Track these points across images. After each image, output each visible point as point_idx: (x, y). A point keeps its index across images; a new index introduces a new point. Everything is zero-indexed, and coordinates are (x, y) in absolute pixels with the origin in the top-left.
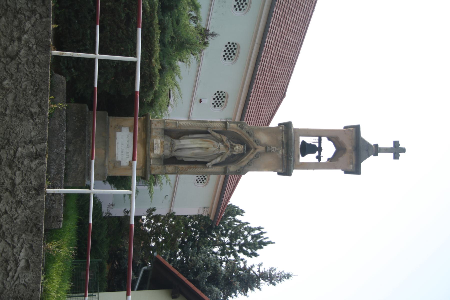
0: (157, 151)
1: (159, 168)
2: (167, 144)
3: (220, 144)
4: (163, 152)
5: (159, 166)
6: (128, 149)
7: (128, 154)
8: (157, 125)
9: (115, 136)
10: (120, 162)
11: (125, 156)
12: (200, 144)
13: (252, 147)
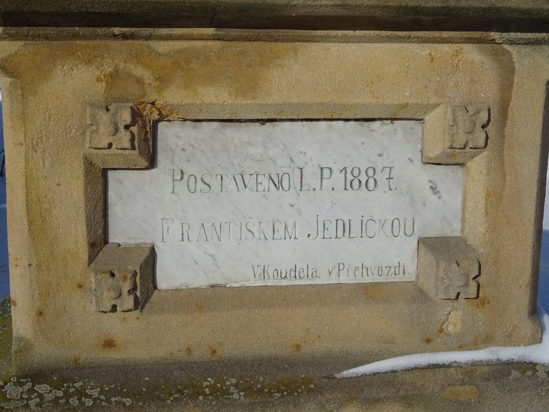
6: (312, 180)
7: (359, 180)
11: (380, 203)
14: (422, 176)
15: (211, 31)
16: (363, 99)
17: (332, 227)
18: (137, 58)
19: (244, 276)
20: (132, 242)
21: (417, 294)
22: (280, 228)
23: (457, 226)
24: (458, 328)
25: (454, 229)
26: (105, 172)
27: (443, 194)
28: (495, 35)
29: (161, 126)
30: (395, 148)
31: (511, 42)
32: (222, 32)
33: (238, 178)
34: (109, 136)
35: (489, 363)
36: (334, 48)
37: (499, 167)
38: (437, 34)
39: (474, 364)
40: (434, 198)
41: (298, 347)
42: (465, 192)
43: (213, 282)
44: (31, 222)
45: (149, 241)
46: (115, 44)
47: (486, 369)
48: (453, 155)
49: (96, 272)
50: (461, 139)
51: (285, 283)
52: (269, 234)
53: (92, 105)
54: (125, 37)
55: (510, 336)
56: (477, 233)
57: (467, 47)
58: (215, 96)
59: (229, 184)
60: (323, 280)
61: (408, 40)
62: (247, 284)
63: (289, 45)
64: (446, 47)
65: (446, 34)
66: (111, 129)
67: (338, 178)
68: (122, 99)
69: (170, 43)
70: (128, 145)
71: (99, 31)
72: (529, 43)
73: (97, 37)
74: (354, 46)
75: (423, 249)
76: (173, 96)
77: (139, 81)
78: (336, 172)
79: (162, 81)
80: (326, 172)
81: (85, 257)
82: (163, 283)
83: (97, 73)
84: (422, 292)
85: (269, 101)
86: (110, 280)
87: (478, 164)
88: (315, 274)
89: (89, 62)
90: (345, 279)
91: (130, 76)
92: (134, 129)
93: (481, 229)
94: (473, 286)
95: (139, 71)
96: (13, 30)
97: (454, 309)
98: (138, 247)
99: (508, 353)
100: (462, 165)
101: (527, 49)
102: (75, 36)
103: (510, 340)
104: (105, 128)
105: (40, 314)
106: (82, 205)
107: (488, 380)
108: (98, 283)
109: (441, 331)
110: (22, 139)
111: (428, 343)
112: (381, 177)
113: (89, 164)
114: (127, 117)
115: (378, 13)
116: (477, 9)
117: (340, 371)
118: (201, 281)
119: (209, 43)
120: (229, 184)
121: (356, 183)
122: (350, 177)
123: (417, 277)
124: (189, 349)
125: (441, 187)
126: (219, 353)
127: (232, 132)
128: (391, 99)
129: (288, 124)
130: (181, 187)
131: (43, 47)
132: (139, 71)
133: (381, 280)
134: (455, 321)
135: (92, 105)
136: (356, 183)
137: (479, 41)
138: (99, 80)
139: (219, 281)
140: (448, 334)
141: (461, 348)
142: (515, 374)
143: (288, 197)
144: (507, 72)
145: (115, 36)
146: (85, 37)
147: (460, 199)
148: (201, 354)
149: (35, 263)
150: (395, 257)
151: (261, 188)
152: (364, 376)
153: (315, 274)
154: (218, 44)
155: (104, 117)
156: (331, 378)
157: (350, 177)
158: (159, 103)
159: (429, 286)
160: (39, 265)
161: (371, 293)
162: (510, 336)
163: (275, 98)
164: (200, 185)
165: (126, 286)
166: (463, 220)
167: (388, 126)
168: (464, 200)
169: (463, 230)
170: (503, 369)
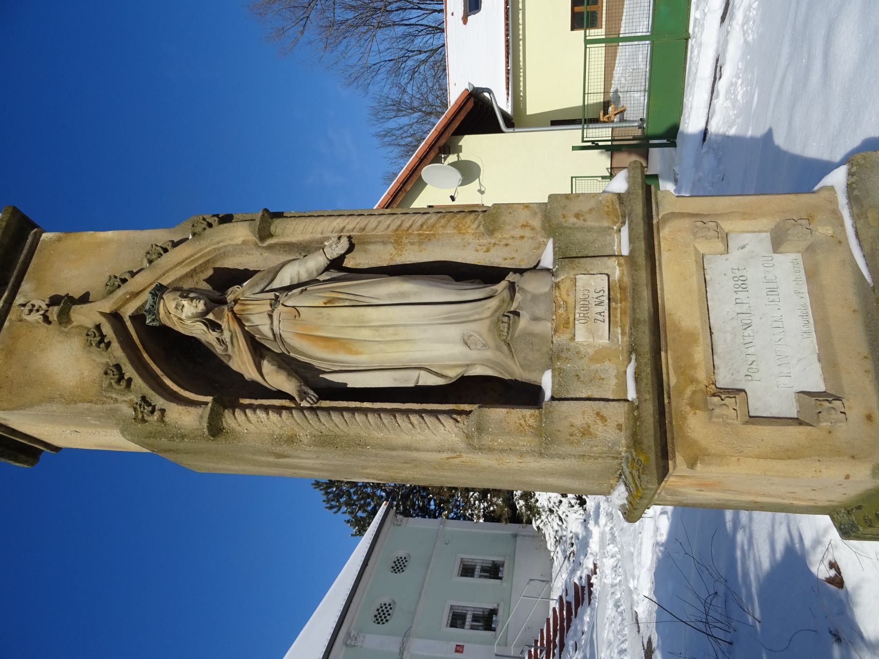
0: (592, 285)
1: (577, 216)
2: (536, 319)
3: (266, 330)
4: (557, 286)
5: (579, 223)
6: (744, 308)
7: (742, 284)
8: (590, 419)
9: (828, 360)
10: (778, 243)
11: (754, 274)
12: (362, 325)
13: (129, 324)
14: (735, 254)
15: (663, 354)
16: (694, 281)
17: (772, 298)
18: (681, 393)
19: (811, 342)
20: (795, 404)
21: (810, 250)
22: (776, 324)
23: (764, 235)
24: (829, 228)
25: (766, 237)
26: (750, 417)
27: (745, 243)
28: (655, 221)
29: (718, 386)
30: (720, 269)
31: (658, 214)
32: (663, 348)
33: (747, 346)
34: (729, 408)
35: (851, 208)
36: (666, 296)
37: (728, 215)
38: (656, 247)
39: (852, 215)
40: (748, 247)
41: (854, 311)
42: (743, 232)
43: (817, 360)
44: (789, 458)
45: (793, 395)
46: (673, 404)
47: (855, 209)
48: (722, 237)
49: (819, 422)
50: (713, 233)
51: (812, 321)
52: (780, 330)
53: (711, 418)
54: (669, 398)
55: (831, 202)
56: (767, 223)
57: (661, 234)
58: (699, 354)
59: (750, 351)
60: (807, 300)
61: (660, 260)
62: (815, 341)
63: (667, 320)
64: (662, 244)
65: (656, 243)
66: (724, 407)
67: (741, 295)
68: (706, 403)
69: (671, 376)
70: (733, 400)
71: (667, 410)
72: (657, 206)
73: (670, 411)
74: (665, 287)
75: (780, 250)
76: (701, 375)
77: (694, 393)
78: (737, 296)
79: (693, 381)
80: (738, 301)
81: (809, 428)
82: (822, 388)
83: (691, 414)
84: (808, 248)
85: (700, 327)
86: (824, 414)
87: (726, 225)
88: (805, 306)
89: (685, 418)
90: (805, 289)
91: (691, 397)
92: (723, 397)
93: (765, 221)
94: (800, 222)
95: (688, 392)
96: (670, 455)
97: (817, 230)
98: (798, 401)
99: (842, 200)
100: (727, 235)
101: (661, 208)
102: (671, 423)
103: (834, 201)
104: (725, 411)
105: (853, 457)
106: (774, 428)
107: (862, 206)
108: (826, 421)
109: (832, 236)
110: (735, 459)
111: (841, 242)
112: (738, 274)
113: (746, 423)
114: (716, 399)
115: (649, 270)
116: (644, 225)
117: (869, 285)
118: (817, 367)
119: (669, 356)
120: (750, 351)
121: (743, 286)
122: (740, 289)
123: (799, 252)
124: (866, 371)
125: (741, 244)
126: (866, 355)
127: (720, 348)
128: (693, 267)
129: (711, 321)
130: (756, 376)
131: (678, 442)
132: (688, 392)
133: (803, 271)
134: (825, 230)
135: (711, 418)
136: (743, 286)
137: (658, 228)
138: (695, 414)
139: (815, 357)
140: (834, 232)
141: (842, 225)
142: (856, 193)
143: (756, 321)
144: (673, 215)
145: (669, 402)
146: (671, 418)
147: (747, 234)
148: (868, 365)
149: (817, 458)
150: (787, 267)
151: (751, 334)
152: (870, 271)
153: (805, 306)
154: (669, 352)
155: (717, 411)
156: (874, 289)
157: (740, 289)
158: (706, 383)
159: (803, 245)
160: (819, 455)
161: (812, 275)
162: (831, 202)
163: (698, 324)
164: (753, 366)
165: (827, 404)
166: (759, 232)
167: (708, 271)
168: (747, 232)
169: (766, 232)
170: (853, 199)
